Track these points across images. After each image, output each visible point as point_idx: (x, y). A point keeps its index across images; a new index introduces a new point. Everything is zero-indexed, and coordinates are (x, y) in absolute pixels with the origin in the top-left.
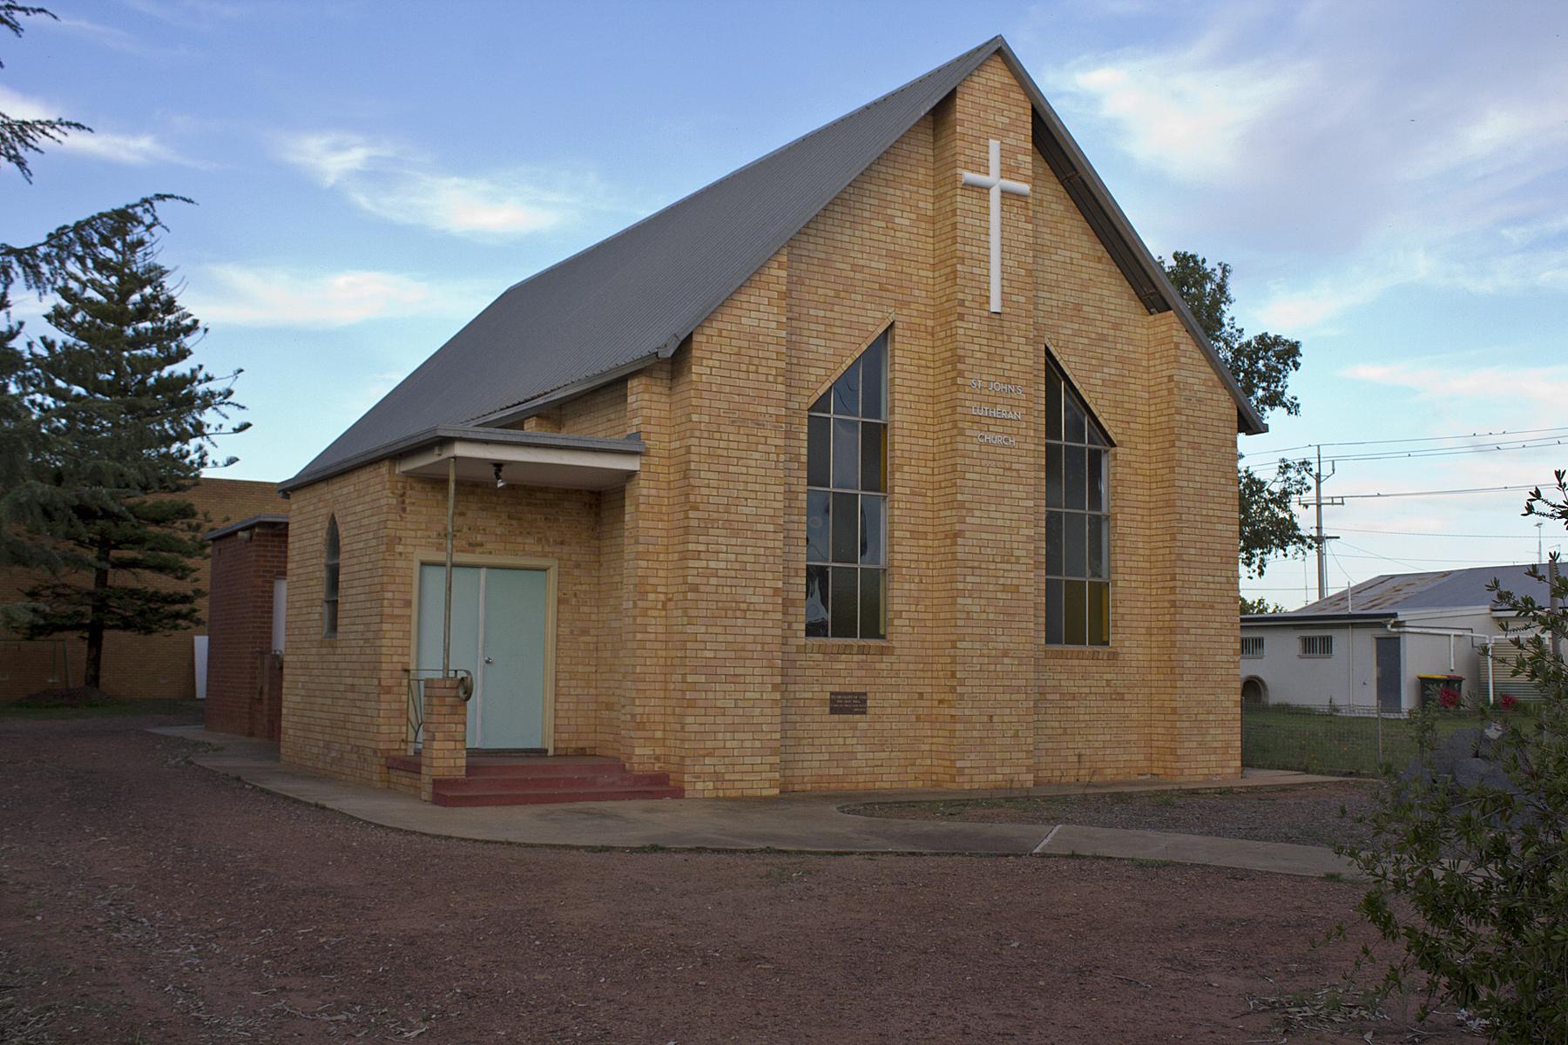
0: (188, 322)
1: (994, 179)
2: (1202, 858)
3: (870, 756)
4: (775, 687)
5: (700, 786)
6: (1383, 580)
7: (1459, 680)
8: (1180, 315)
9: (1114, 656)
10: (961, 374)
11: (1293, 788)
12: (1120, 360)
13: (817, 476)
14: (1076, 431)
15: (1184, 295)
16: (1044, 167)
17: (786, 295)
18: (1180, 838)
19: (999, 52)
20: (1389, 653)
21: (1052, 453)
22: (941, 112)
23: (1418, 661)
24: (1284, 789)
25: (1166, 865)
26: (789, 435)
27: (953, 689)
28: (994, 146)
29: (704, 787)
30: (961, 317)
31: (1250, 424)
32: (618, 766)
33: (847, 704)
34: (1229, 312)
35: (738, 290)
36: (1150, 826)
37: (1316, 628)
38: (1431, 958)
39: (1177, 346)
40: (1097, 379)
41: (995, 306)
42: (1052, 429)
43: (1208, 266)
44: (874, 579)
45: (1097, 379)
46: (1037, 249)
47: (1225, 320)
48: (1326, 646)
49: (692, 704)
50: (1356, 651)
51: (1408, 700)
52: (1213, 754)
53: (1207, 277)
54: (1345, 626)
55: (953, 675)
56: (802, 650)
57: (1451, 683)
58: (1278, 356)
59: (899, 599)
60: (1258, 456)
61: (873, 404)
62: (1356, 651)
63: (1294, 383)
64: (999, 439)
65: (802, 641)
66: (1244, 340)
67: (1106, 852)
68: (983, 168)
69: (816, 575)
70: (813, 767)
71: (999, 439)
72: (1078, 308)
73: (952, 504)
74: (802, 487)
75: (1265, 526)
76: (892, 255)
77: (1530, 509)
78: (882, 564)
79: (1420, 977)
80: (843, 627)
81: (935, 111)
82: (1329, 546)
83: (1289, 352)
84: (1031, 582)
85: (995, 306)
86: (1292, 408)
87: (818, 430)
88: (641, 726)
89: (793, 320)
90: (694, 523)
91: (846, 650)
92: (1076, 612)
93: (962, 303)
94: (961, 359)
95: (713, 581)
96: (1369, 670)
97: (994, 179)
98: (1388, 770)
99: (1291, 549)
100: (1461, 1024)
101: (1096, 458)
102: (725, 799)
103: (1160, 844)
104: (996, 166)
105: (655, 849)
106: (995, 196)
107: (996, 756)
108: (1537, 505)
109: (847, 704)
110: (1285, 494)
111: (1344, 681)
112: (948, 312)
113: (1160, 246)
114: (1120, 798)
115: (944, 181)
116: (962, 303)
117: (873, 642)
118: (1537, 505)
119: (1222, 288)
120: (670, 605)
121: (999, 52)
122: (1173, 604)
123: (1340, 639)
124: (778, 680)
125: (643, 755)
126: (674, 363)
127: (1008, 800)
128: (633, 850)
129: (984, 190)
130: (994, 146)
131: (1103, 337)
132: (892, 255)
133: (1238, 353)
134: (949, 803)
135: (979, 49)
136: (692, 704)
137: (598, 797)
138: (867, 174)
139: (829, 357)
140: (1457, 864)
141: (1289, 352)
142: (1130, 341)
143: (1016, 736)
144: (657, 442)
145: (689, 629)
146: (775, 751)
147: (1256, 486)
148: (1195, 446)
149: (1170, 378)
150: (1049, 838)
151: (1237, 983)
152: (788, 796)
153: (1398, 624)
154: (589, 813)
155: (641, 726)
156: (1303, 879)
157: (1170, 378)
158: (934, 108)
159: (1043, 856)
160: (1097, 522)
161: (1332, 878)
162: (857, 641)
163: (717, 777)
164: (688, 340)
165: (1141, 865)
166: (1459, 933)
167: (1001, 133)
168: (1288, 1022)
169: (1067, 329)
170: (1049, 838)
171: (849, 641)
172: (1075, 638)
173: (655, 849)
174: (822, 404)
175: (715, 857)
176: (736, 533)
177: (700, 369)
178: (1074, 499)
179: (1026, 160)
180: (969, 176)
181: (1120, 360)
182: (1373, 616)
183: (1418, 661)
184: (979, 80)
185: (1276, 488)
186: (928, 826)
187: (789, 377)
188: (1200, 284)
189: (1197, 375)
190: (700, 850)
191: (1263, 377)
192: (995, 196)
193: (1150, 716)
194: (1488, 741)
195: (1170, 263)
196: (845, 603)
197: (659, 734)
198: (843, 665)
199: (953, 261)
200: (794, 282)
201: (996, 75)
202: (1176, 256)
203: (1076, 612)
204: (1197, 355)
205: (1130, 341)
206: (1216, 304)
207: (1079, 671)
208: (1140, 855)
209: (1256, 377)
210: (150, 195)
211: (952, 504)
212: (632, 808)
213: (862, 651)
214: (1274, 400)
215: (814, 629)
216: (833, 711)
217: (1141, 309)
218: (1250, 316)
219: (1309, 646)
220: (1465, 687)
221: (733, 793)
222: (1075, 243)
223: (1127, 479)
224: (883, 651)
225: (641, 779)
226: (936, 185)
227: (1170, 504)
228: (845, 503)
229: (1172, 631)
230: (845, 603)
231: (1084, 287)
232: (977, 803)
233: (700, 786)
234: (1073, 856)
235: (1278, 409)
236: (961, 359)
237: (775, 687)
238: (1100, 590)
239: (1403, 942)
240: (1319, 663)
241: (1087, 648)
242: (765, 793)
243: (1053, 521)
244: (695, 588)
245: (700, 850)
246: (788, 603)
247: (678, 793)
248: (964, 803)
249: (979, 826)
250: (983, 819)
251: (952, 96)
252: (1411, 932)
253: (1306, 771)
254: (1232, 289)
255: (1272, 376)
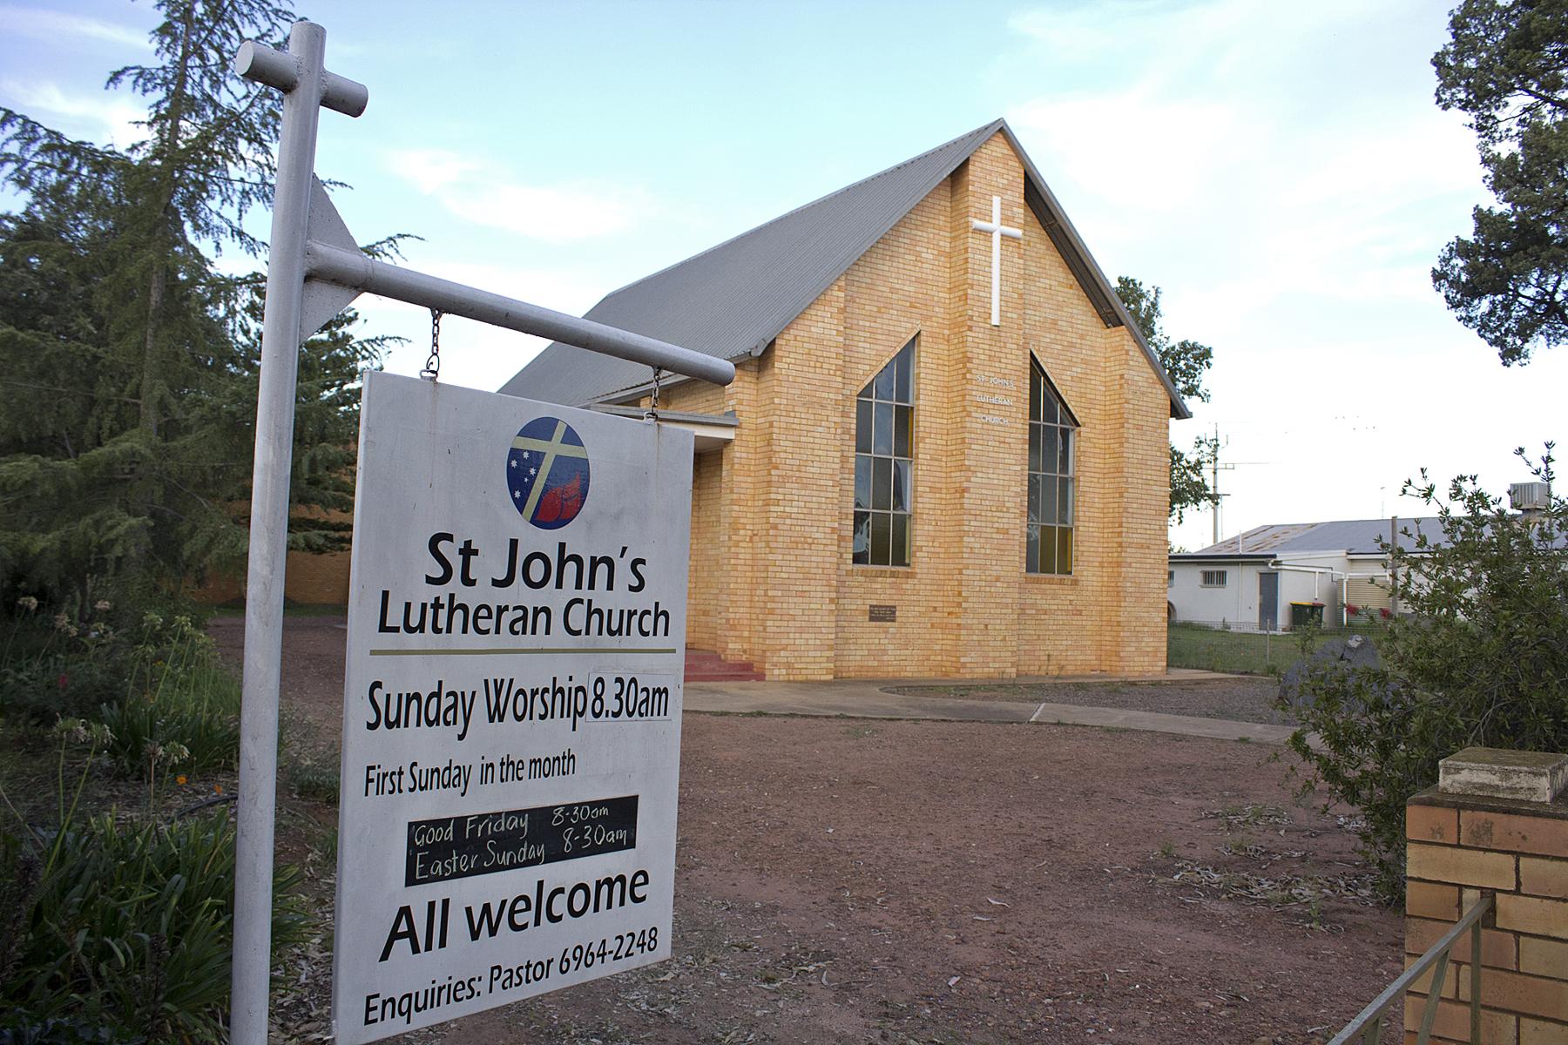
0: (351, 314)
1: (996, 226)
2: (1150, 727)
3: (900, 652)
4: (831, 600)
5: (776, 672)
6: (1265, 529)
7: (1322, 607)
8: (1130, 329)
9: (1075, 582)
10: (969, 371)
11: (1205, 682)
12: (1084, 361)
13: (863, 444)
14: (1050, 416)
15: (1120, 308)
16: (1032, 217)
17: (843, 311)
18: (1134, 713)
19: (1001, 130)
20: (1269, 584)
21: (1034, 430)
22: (958, 176)
23: (1292, 591)
24: (1198, 682)
25: (1126, 730)
26: (844, 414)
27: (959, 605)
28: (996, 200)
29: (779, 673)
30: (970, 328)
31: (1178, 412)
32: (715, 657)
33: (882, 614)
34: (1159, 323)
35: (809, 307)
36: (1107, 705)
37: (1213, 566)
38: (1332, 773)
39: (1127, 352)
40: (1067, 375)
41: (995, 320)
42: (1034, 414)
43: (1144, 288)
44: (902, 523)
45: (1067, 375)
46: (1026, 278)
47: (1156, 329)
48: (1222, 578)
49: (772, 612)
50: (1244, 583)
51: (1283, 619)
52: (1145, 657)
53: (1142, 296)
54: (1237, 564)
55: (960, 594)
56: (850, 573)
57: (1315, 608)
58: (1196, 358)
59: (921, 537)
60: (1181, 435)
61: (903, 393)
62: (1244, 583)
63: (1206, 379)
64: (996, 420)
65: (850, 567)
66: (1169, 345)
67: (1078, 721)
68: (987, 216)
69: (859, 518)
70: (857, 659)
71: (996, 420)
72: (1055, 322)
73: (961, 468)
74: (852, 452)
75: (1188, 489)
76: (919, 281)
77: (1404, 492)
78: (908, 511)
79: (1323, 785)
80: (880, 557)
81: (953, 174)
82: (1223, 501)
83: (1204, 355)
84: (1014, 524)
85: (995, 320)
86: (1205, 397)
87: (863, 410)
88: (733, 627)
89: (848, 329)
90: (775, 479)
91: (882, 574)
92: (1049, 552)
93: (971, 318)
94: (970, 360)
95: (788, 521)
96: (1254, 599)
97: (996, 226)
98: (1272, 670)
99: (1202, 504)
100: (1340, 827)
101: (1065, 434)
102: (795, 682)
103: (1118, 717)
104: (997, 213)
105: (760, 714)
106: (996, 238)
107: (989, 655)
108: (1409, 489)
109: (882, 614)
110: (1199, 463)
111: (1234, 605)
112: (961, 324)
113: (1112, 271)
114: (1080, 687)
115: (959, 225)
116: (971, 318)
117: (901, 569)
118: (1409, 489)
119: (1154, 305)
120: (756, 539)
121: (1001, 131)
122: (1120, 545)
123: (1232, 573)
124: (833, 595)
125: (734, 649)
126: (760, 361)
127: (1000, 686)
128: (746, 715)
129: (988, 234)
130: (996, 200)
131: (1072, 345)
132: (919, 281)
133: (1165, 354)
134: (957, 688)
135: (986, 128)
136: (772, 612)
137: (703, 679)
138: (903, 222)
139: (873, 357)
140: (1354, 714)
141: (1204, 355)
142: (1092, 348)
143: (1004, 640)
144: (748, 417)
145: (771, 557)
146: (830, 648)
147: (1176, 456)
148: (1139, 427)
149: (1122, 376)
150: (1039, 711)
151: (1190, 802)
152: (839, 681)
153: (1277, 563)
154: (701, 689)
155: (733, 627)
156: (1223, 741)
157: (1122, 376)
158: (952, 175)
159: (1037, 723)
160: (1065, 483)
161: (1243, 740)
162: (889, 568)
163: (789, 666)
164: (773, 342)
165: (1108, 730)
166: (1351, 757)
167: (1002, 191)
168: (1229, 824)
169: (1047, 338)
170: (1039, 711)
171: (883, 567)
172: (1047, 569)
173: (760, 714)
174: (866, 392)
175: (804, 721)
176: (805, 486)
177: (780, 366)
178: (1049, 466)
179: (1020, 211)
180: (977, 223)
181: (1084, 361)
182: (1257, 559)
183: (1292, 591)
184: (986, 151)
185: (1193, 459)
186: (950, 703)
187: (843, 370)
188: (1137, 301)
189: (1141, 374)
190: (793, 715)
191: (1183, 373)
192: (996, 238)
193: (1105, 626)
194: (1350, 649)
195: (1115, 284)
196: (883, 541)
197: (746, 634)
198: (880, 585)
199: (963, 288)
200: (850, 300)
201: (999, 148)
202: (1120, 280)
203: (1049, 552)
204: (1142, 359)
205: (1092, 348)
206: (1149, 317)
207: (1050, 593)
208: (1107, 724)
209: (1180, 370)
210: (393, 234)
211: (961, 468)
212: (731, 687)
213: (893, 574)
214: (1191, 391)
215: (858, 558)
216: (871, 619)
217: (1101, 324)
218: (1171, 330)
219: (1208, 578)
220: (1326, 615)
221: (800, 678)
222: (1054, 275)
223: (1088, 451)
224: (908, 576)
225: (733, 666)
226: (953, 229)
227: (1119, 470)
228: (882, 464)
229: (1119, 565)
230: (883, 541)
231: (1059, 307)
232: (978, 688)
233: (776, 672)
234: (1059, 724)
235: (1195, 398)
236: (970, 360)
237: (831, 600)
238: (1066, 534)
239: (1315, 764)
240: (1215, 592)
241: (1056, 576)
242: (824, 678)
243: (1033, 484)
244: (775, 527)
245: (793, 715)
246: (841, 539)
247: (760, 677)
248: (969, 688)
249: (987, 703)
250: (984, 698)
251: (966, 163)
252: (1320, 758)
253: (1213, 670)
254: (1161, 307)
255: (1190, 373)
